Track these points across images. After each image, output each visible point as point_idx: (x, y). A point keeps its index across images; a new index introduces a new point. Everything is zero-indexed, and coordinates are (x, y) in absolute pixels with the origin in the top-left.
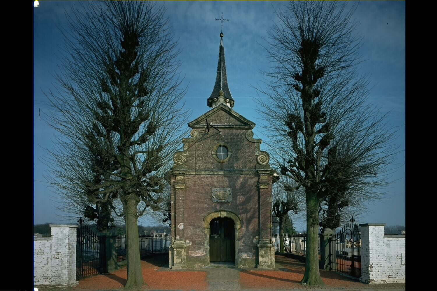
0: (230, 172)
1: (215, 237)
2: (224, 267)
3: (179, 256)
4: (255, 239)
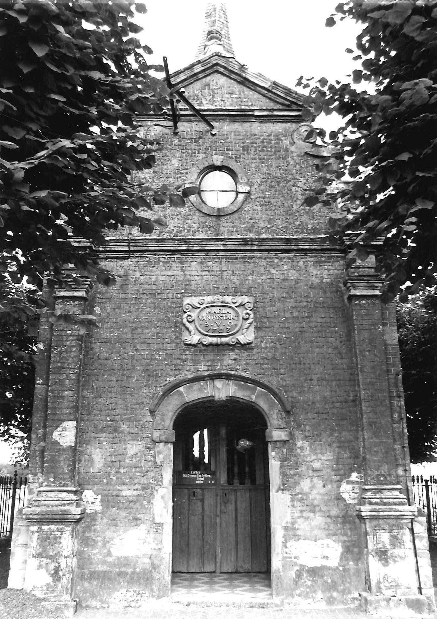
0: (246, 245)
1: (195, 479)
2: (46, 382)
3: (47, 557)
4: (348, 483)
